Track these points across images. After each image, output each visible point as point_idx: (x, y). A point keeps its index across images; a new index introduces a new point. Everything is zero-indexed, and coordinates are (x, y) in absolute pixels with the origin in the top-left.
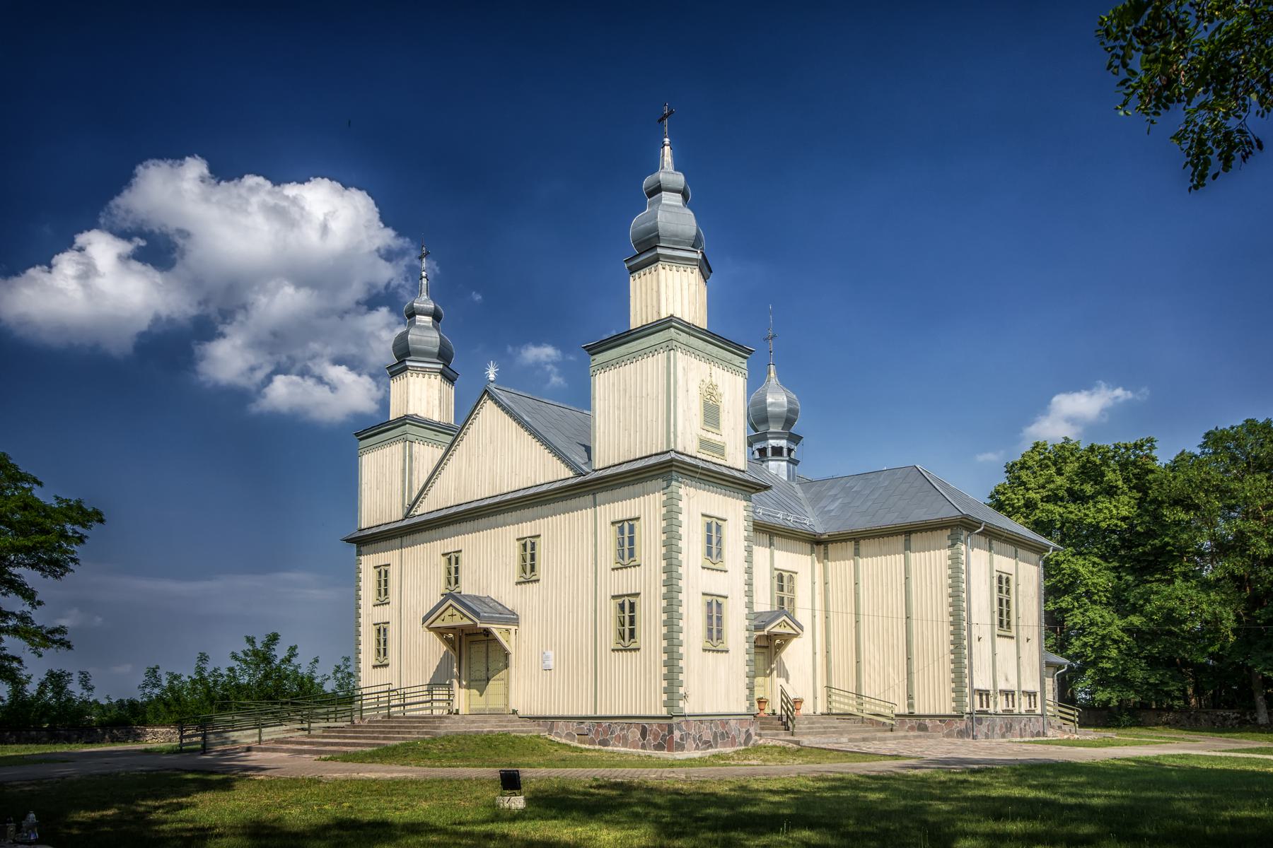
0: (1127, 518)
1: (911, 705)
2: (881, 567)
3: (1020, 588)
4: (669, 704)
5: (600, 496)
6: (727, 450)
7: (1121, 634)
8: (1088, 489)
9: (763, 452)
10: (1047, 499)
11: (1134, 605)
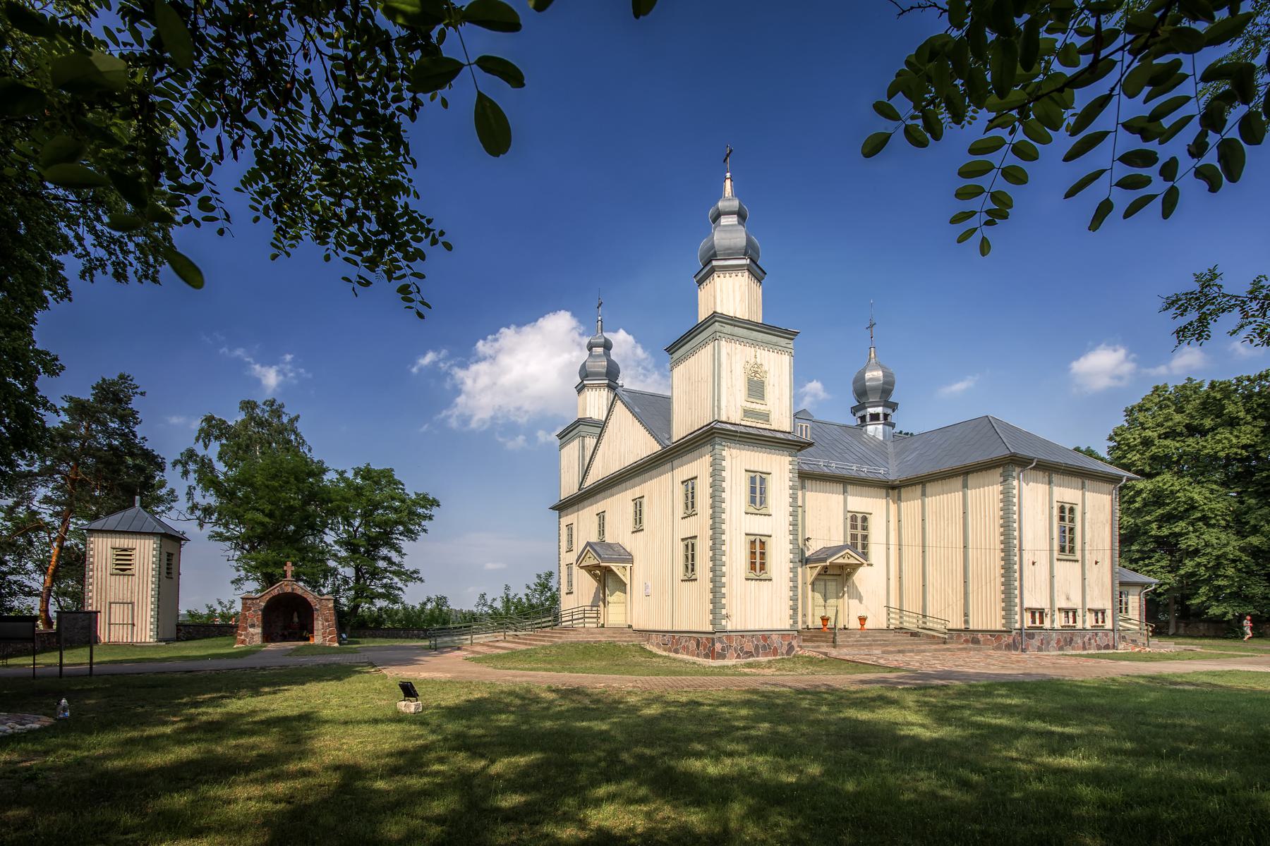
0: (1250, 446)
1: (966, 622)
2: (943, 503)
3: (1088, 516)
4: (713, 623)
5: (675, 463)
6: (772, 417)
7: (1238, 553)
8: (1208, 423)
9: (863, 418)
10: (1166, 436)
11: (1255, 526)
